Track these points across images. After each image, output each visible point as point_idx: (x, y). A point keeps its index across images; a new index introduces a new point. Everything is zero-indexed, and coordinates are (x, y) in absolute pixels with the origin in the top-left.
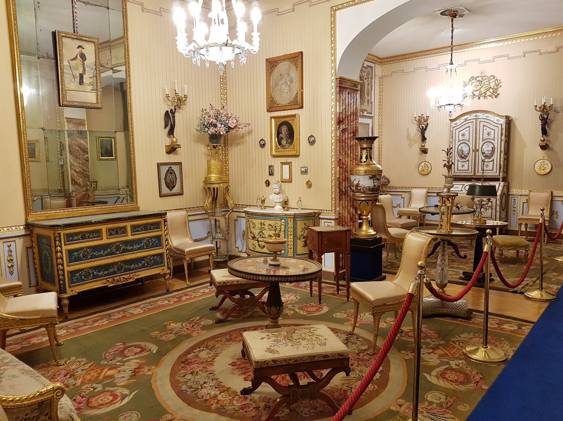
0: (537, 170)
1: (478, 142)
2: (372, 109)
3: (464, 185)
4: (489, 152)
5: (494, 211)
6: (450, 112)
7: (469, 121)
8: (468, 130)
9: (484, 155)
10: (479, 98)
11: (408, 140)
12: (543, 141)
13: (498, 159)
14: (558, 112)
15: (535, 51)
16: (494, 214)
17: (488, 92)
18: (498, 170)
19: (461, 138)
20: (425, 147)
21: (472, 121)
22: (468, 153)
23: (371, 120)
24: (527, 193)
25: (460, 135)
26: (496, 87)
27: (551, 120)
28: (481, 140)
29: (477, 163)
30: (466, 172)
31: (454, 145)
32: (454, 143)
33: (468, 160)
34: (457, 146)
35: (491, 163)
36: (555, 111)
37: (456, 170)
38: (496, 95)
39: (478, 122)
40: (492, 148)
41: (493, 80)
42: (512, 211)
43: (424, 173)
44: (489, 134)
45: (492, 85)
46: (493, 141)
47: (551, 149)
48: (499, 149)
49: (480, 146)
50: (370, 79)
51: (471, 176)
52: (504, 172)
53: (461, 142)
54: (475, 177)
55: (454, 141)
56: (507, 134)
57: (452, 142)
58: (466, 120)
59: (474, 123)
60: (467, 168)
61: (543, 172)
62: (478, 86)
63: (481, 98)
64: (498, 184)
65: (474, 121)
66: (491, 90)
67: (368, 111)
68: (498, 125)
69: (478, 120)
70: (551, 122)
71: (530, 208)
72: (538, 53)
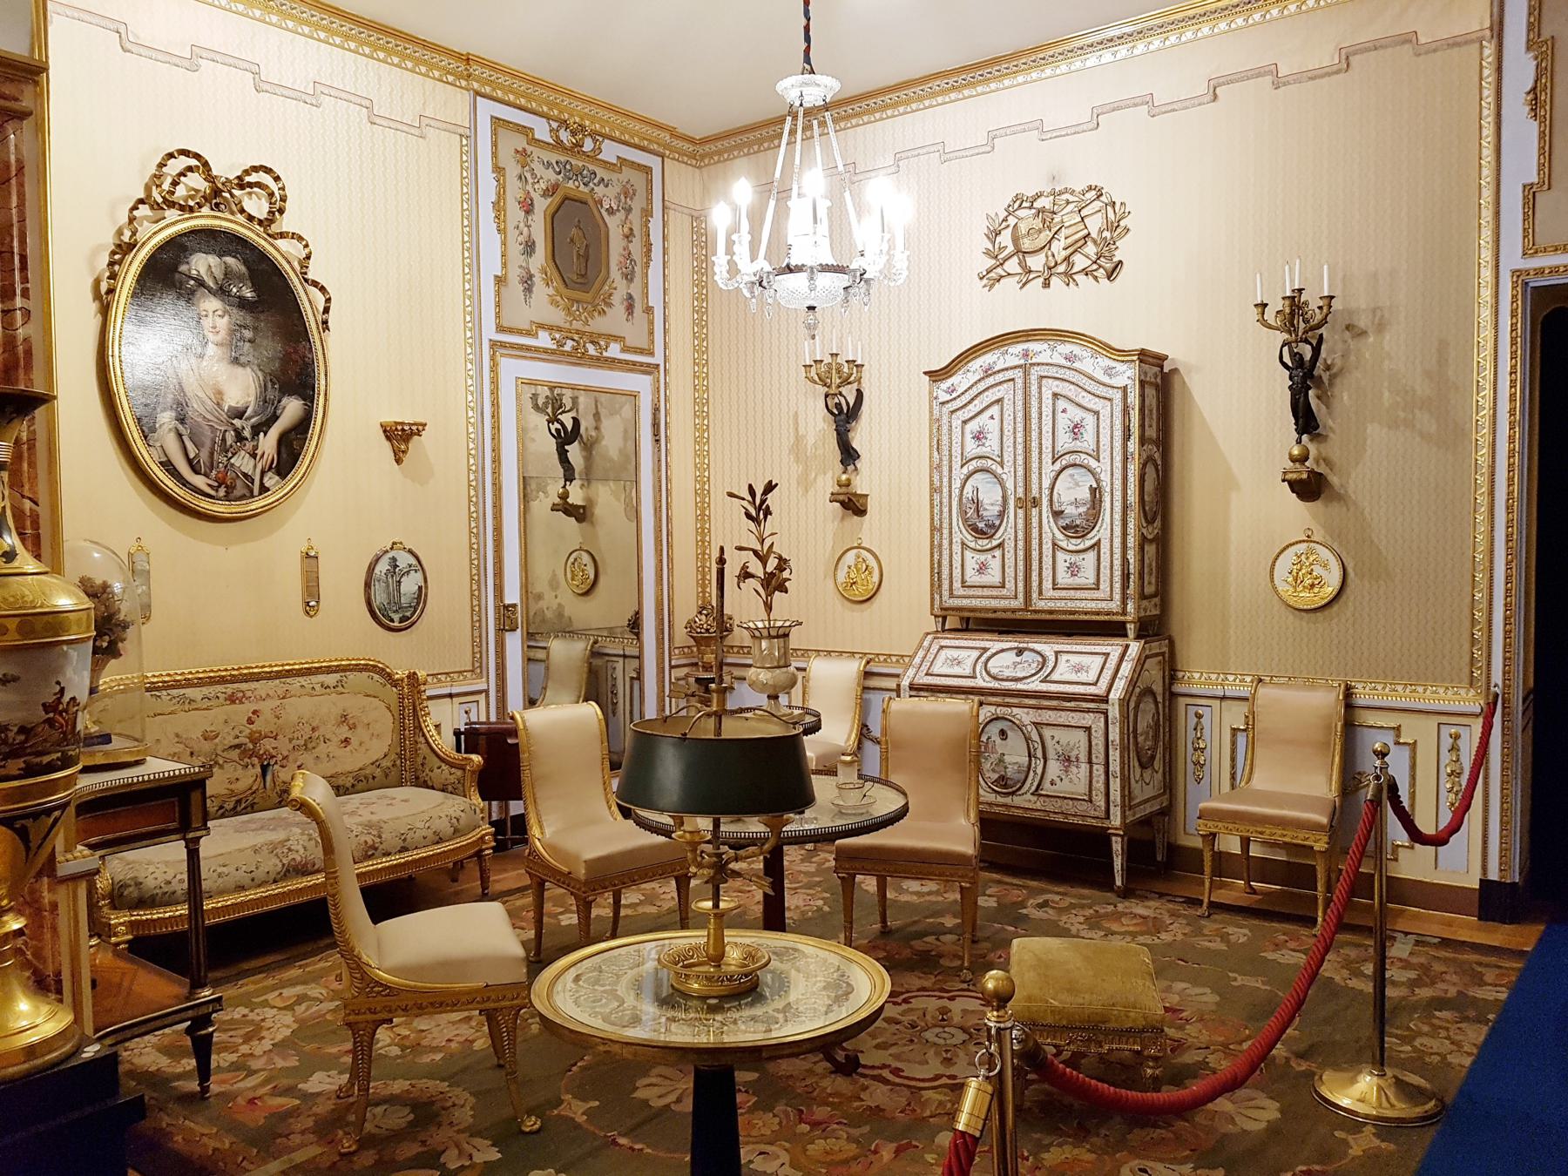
0: (1281, 587)
1: (1035, 465)
2: (651, 333)
3: (985, 650)
4: (1082, 510)
5: (1099, 770)
6: (811, 308)
7: (999, 377)
8: (997, 417)
9: (1062, 523)
10: (1046, 284)
11: (797, 460)
12: (1303, 459)
13: (1117, 542)
14: (1363, 333)
15: (1258, 73)
16: (1099, 784)
17: (1077, 258)
18: (1117, 586)
19: (972, 448)
20: (852, 489)
21: (1009, 375)
22: (1002, 514)
23: (647, 379)
24: (1244, 691)
25: (968, 436)
26: (1107, 234)
27: (1335, 370)
28: (1047, 458)
29: (1035, 554)
30: (995, 592)
31: (945, 480)
32: (945, 469)
33: (1000, 545)
34: (957, 484)
35: (1091, 555)
36: (1348, 327)
37: (957, 585)
38: (1109, 266)
39: (1033, 379)
40: (1093, 491)
41: (1097, 205)
42: (1190, 767)
43: (860, 592)
44: (1076, 430)
45: (1095, 224)
46: (1093, 463)
47: (1338, 497)
48: (1118, 495)
49: (1046, 483)
50: (635, 217)
51: (1014, 611)
52: (1143, 596)
53: (973, 465)
54: (1029, 616)
55: (945, 463)
56: (1151, 433)
57: (939, 466)
58: (989, 372)
59: (1019, 382)
60: (997, 579)
61: (1308, 599)
62: (1040, 231)
63: (1055, 281)
64: (1120, 650)
65: (1018, 374)
66: (1091, 249)
67: (629, 342)
68: (1110, 393)
69: (1035, 372)
70: (1333, 378)
71: (1257, 762)
72: (1269, 79)
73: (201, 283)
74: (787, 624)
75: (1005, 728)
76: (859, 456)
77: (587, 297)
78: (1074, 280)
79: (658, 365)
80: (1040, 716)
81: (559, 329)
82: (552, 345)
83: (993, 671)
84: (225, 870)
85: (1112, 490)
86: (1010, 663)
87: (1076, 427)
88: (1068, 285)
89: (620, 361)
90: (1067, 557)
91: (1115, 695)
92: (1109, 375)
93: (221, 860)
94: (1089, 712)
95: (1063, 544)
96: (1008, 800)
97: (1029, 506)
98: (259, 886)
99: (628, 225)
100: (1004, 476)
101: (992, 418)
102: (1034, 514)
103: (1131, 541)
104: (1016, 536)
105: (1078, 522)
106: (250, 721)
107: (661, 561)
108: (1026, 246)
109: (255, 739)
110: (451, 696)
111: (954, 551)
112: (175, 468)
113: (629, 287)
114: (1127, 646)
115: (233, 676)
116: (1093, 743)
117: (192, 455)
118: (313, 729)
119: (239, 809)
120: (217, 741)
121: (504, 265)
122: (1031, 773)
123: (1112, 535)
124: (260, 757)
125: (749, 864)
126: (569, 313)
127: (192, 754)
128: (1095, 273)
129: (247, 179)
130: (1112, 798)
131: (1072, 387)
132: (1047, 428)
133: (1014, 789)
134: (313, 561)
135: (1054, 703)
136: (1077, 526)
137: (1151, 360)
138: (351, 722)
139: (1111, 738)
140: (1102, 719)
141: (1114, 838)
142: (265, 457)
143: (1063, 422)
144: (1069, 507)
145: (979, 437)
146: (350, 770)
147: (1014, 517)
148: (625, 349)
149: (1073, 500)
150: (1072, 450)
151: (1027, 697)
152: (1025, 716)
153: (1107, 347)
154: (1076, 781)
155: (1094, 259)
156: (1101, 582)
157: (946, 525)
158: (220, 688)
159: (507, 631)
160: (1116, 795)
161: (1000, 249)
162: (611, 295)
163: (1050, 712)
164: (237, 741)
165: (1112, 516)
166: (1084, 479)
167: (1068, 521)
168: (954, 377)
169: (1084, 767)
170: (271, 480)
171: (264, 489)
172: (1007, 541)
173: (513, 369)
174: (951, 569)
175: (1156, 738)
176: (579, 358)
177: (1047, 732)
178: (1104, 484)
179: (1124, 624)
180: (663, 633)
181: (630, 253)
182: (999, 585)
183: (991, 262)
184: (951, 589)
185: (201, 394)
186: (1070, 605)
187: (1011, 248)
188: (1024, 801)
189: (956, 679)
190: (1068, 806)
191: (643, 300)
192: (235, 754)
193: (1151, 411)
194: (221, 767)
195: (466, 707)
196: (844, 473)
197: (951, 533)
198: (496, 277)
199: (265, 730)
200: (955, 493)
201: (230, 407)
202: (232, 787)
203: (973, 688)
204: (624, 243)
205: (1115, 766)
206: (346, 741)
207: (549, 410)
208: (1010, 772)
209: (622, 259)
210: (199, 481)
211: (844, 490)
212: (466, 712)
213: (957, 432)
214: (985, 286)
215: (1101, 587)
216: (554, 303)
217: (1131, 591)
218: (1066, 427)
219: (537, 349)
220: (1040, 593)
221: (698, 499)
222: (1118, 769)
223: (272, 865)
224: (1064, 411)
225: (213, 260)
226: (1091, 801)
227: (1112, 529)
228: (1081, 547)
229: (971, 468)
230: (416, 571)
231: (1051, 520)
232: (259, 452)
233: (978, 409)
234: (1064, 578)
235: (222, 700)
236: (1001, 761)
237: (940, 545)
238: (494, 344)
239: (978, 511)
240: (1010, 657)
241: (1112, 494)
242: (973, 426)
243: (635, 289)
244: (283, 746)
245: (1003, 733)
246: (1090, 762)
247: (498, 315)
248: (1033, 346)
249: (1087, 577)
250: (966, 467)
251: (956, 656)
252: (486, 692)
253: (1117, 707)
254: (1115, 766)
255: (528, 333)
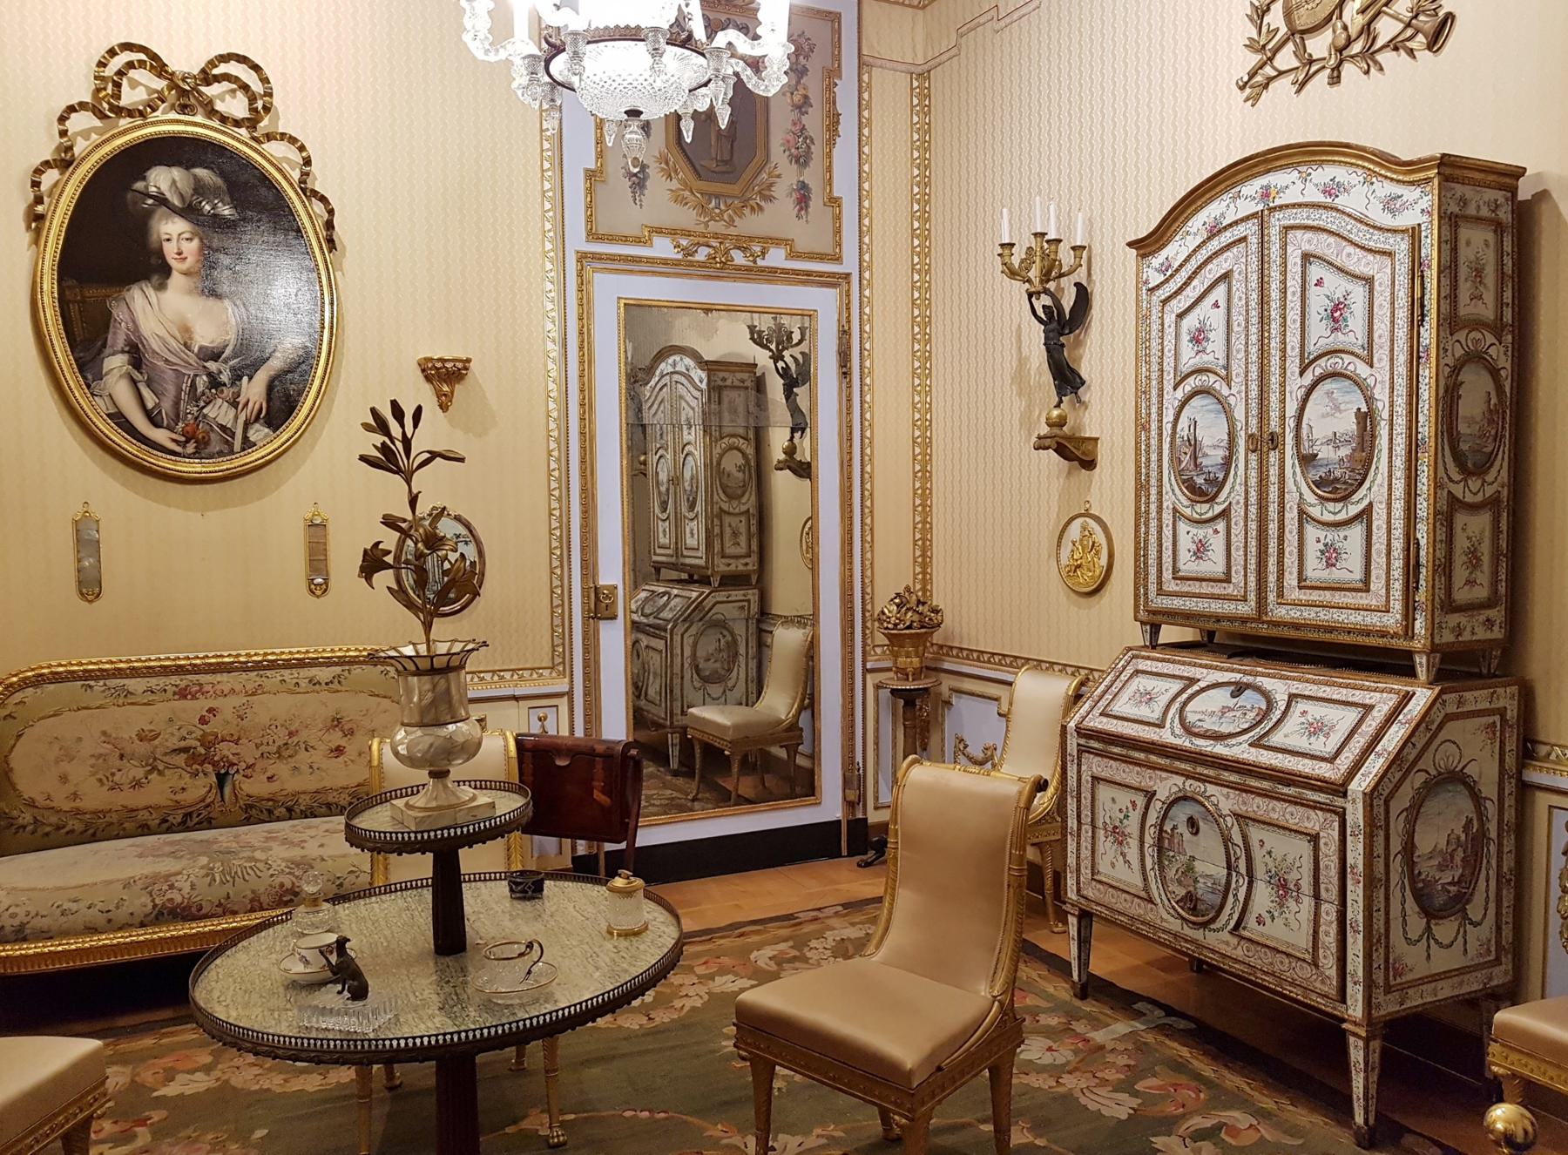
2: (838, 231)
4: (1345, 451)
5: (1329, 912)
7: (1226, 237)
8: (1222, 304)
9: (1315, 474)
10: (1335, 79)
11: (1020, 394)
16: (1329, 938)
18: (1397, 586)
19: (1189, 358)
23: (832, 294)
25: (1185, 338)
28: (1293, 366)
29: (1273, 528)
30: (1217, 589)
31: (1154, 410)
34: (1169, 417)
35: (1357, 531)
39: (1274, 233)
43: (1086, 579)
46: (1362, 370)
49: (1291, 408)
52: (1449, 605)
53: (1191, 384)
54: (1264, 630)
59: (1254, 241)
60: (1219, 568)
63: (1349, 70)
64: (1390, 701)
65: (1250, 229)
69: (1277, 221)
73: (161, 200)
74: (457, 648)
75: (1196, 816)
76: (1083, 383)
77: (735, 189)
78: (1376, 62)
79: (848, 275)
80: (1244, 803)
81: (687, 233)
82: (673, 254)
83: (1191, 718)
84: (74, 907)
85: (1391, 416)
86: (1216, 708)
87: (1336, 308)
88: (1367, 72)
89: (785, 271)
90: (1321, 534)
91: (1360, 785)
92: (1392, 211)
93: (74, 894)
94: (1315, 808)
95: (1315, 512)
96: (1197, 934)
97: (1265, 449)
98: (120, 929)
99: (802, 92)
100: (1232, 400)
101: (1216, 305)
102: (1272, 460)
103: (1423, 508)
104: (1246, 499)
105: (1338, 474)
106: (203, 721)
107: (850, 531)
108: (1302, 21)
109: (209, 742)
110: (516, 698)
111: (1165, 522)
112: (127, 421)
113: (801, 174)
114: (1407, 698)
115: (195, 665)
116: (1322, 865)
117: (150, 405)
118: (291, 734)
119: (190, 824)
120: (156, 742)
121: (600, 155)
122: (1231, 899)
123: (1390, 495)
124: (215, 764)
125: (646, 1010)
126: (703, 209)
127: (122, 757)
128: (1409, 44)
129: (215, 71)
130: (1350, 968)
131: (1332, 239)
132: (1293, 315)
133: (1206, 918)
134: (319, 531)
135: (1265, 785)
136: (1336, 480)
137: (1478, 176)
138: (346, 727)
139: (1350, 861)
140: (1336, 824)
141: (1352, 1039)
142: (250, 405)
143: (1318, 302)
144: (1325, 448)
145: (1198, 338)
146: (344, 784)
147: (1244, 464)
148: (794, 255)
149: (1331, 436)
150: (1329, 348)
151: (1226, 768)
152: (1224, 800)
153: (1387, 161)
154: (1294, 925)
155: (1407, 20)
156: (1373, 578)
157: (1153, 481)
158: (175, 679)
159: (600, 618)
160: (1355, 964)
161: (1269, 31)
162: (771, 185)
163: (1259, 800)
164: (183, 744)
165: (1390, 462)
166: (1347, 398)
167: (1322, 472)
168: (1169, 247)
169: (1307, 903)
170: (258, 433)
171: (247, 444)
172: (1234, 506)
173: (611, 290)
174: (1160, 552)
175: (1473, 861)
176: (720, 269)
177: (1255, 834)
178: (1381, 406)
179: (1409, 654)
180: (853, 627)
181: (803, 128)
182: (1222, 577)
183: (1256, 58)
184: (1160, 583)
185: (163, 333)
186: (1324, 616)
187: (1284, 30)
188: (1218, 940)
189: (1136, 726)
190: (1281, 965)
191: (825, 189)
192: (180, 759)
193: (1479, 272)
194: (160, 773)
195: (541, 713)
196: (1058, 406)
197: (1160, 493)
198: (587, 170)
199: (222, 732)
200: (1167, 429)
201: (201, 348)
202: (178, 797)
203: (1153, 743)
204: (794, 115)
205: (1355, 912)
206: (339, 751)
207: (773, 347)
208: (1202, 889)
209: (790, 137)
210: (161, 436)
211: (1056, 431)
212: (540, 719)
213: (1170, 331)
214: (1247, 100)
215: (1373, 587)
216: (679, 200)
217: (1421, 596)
218: (1322, 311)
219: (650, 261)
220: (1280, 594)
221: (917, 450)
222: (1360, 918)
223: (140, 903)
224: (1319, 283)
225: (176, 173)
226: (1317, 966)
227: (1390, 486)
228: (1342, 516)
229: (1188, 388)
230: (466, 543)
231: (1298, 470)
232: (242, 400)
233: (1197, 293)
234: (1315, 569)
235: (169, 695)
236: (1189, 869)
237: (1148, 512)
238: (582, 257)
239: (1196, 458)
240: (1221, 697)
241: (1391, 425)
242: (1190, 322)
243: (812, 176)
244: (248, 752)
245: (1192, 823)
246: (1317, 896)
247: (589, 219)
248: (1276, 179)
249: (1351, 568)
250: (1180, 389)
251: (1149, 689)
252: (570, 694)
253: (1360, 805)
254: (1355, 912)
255: (638, 241)
